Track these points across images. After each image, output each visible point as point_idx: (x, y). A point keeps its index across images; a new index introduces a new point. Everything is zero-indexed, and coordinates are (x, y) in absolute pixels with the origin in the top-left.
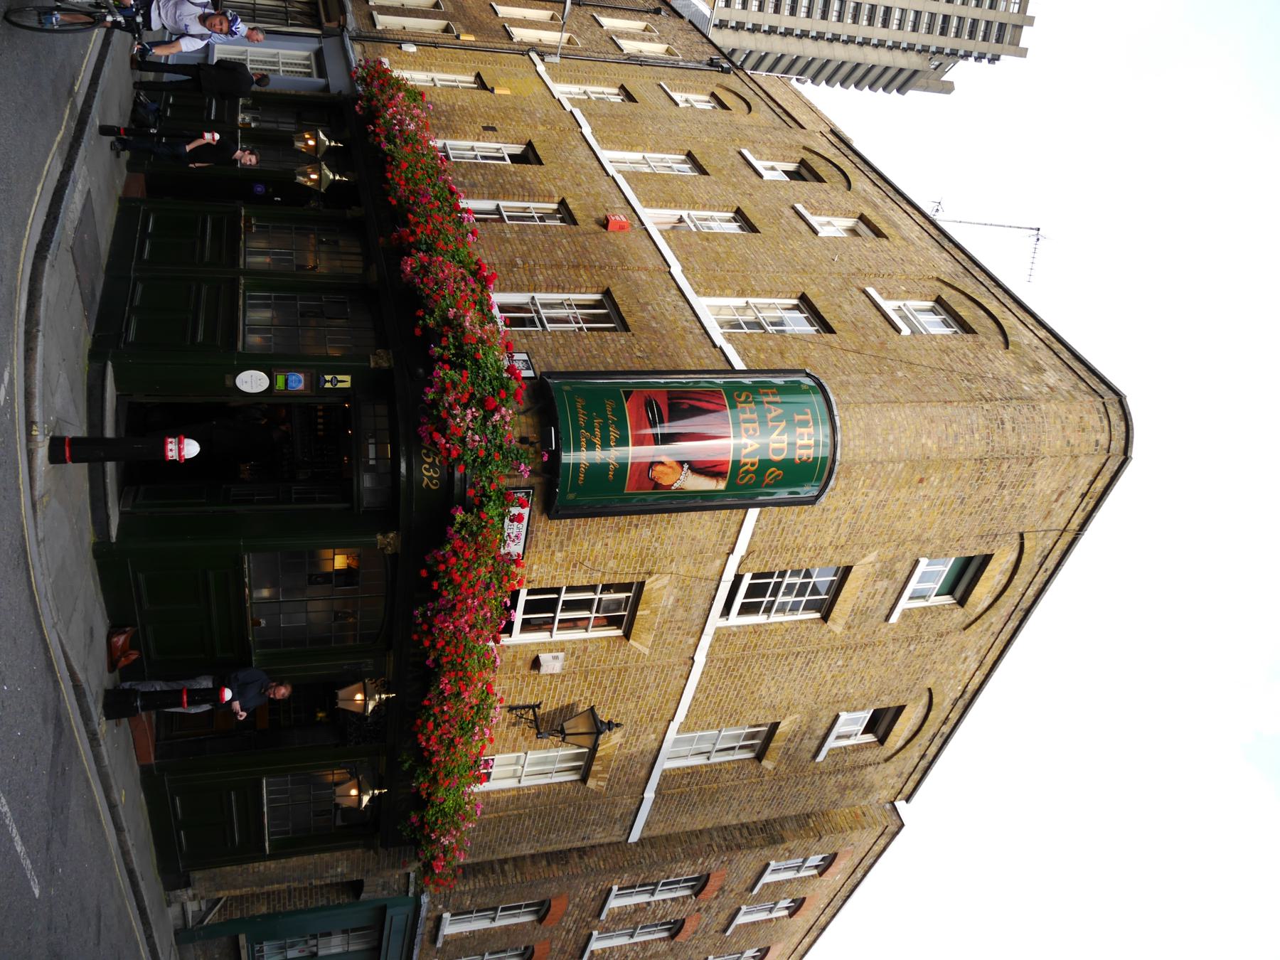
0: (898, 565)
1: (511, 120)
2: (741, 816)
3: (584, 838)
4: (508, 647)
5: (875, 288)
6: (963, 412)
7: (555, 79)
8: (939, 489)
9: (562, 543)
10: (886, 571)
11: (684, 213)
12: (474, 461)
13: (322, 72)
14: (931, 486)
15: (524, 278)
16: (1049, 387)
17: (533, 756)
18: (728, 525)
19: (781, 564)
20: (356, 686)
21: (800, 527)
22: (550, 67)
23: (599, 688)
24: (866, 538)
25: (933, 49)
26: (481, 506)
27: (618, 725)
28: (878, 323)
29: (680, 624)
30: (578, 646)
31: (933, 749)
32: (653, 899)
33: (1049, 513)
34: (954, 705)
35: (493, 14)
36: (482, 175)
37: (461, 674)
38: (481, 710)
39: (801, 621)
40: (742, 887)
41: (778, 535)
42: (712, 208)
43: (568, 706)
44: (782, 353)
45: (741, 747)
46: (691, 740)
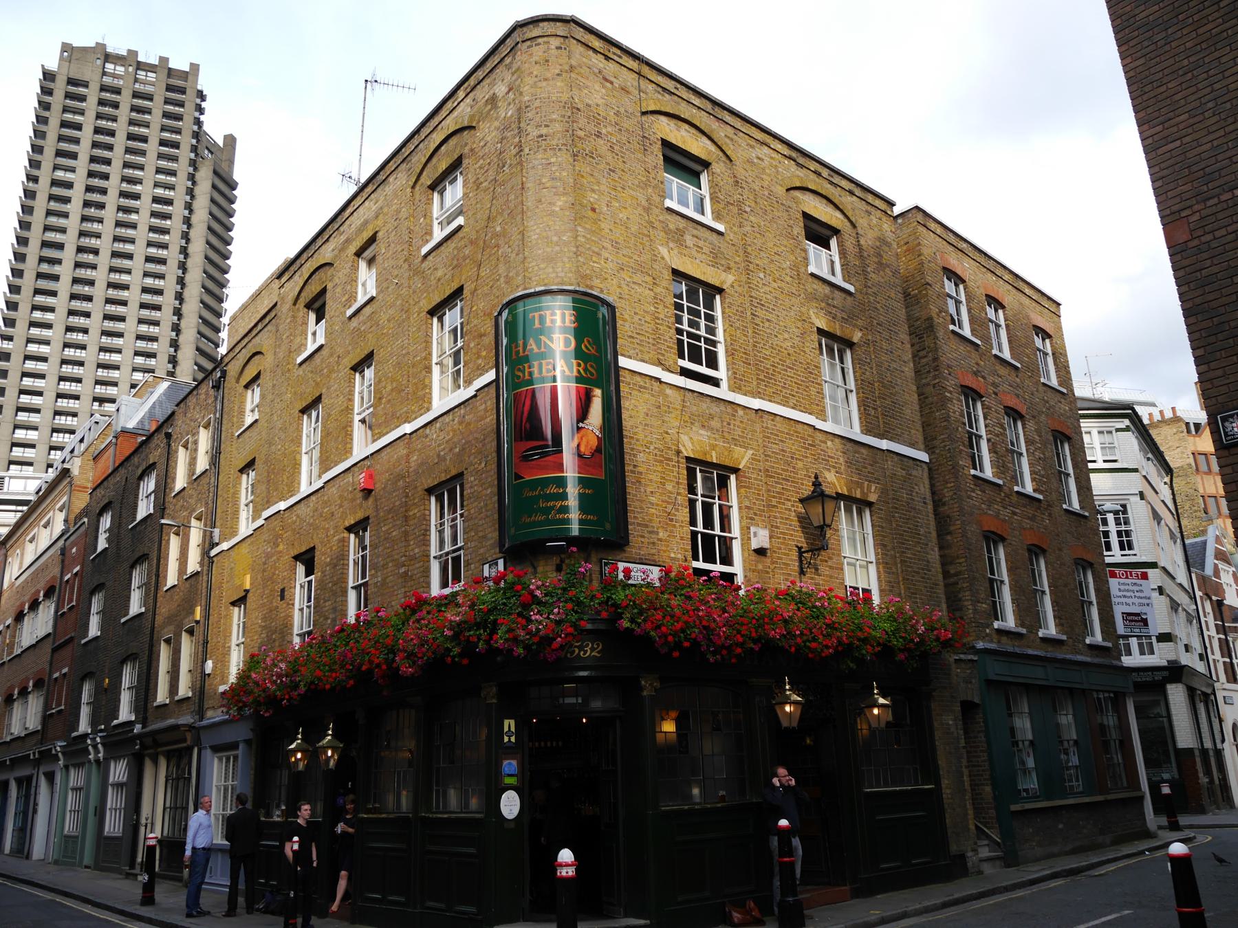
0: (672, 226)
1: (274, 574)
2: (906, 359)
3: (925, 503)
4: (745, 577)
5: (422, 246)
6: (532, 172)
7: (234, 533)
8: (601, 193)
9: (650, 532)
10: (677, 237)
11: (357, 418)
12: (576, 612)
13: (234, 746)
14: (598, 200)
15: (417, 565)
16: (508, 93)
17: (847, 551)
18: (634, 384)
19: (670, 334)
20: (779, 712)
21: (636, 318)
22: (224, 538)
23: (783, 494)
24: (646, 257)
25: (192, 155)
26: (616, 606)
27: (816, 477)
28: (453, 245)
29: (725, 424)
30: (745, 514)
31: (844, 183)
32: (984, 437)
33: (624, 89)
34: (802, 166)
35: (175, 589)
36: (325, 602)
37: (767, 620)
38: (801, 600)
39: (723, 313)
40: (974, 355)
41: (643, 338)
42: (351, 393)
43: (800, 522)
44: (481, 336)
45: (842, 361)
46: (835, 408)
